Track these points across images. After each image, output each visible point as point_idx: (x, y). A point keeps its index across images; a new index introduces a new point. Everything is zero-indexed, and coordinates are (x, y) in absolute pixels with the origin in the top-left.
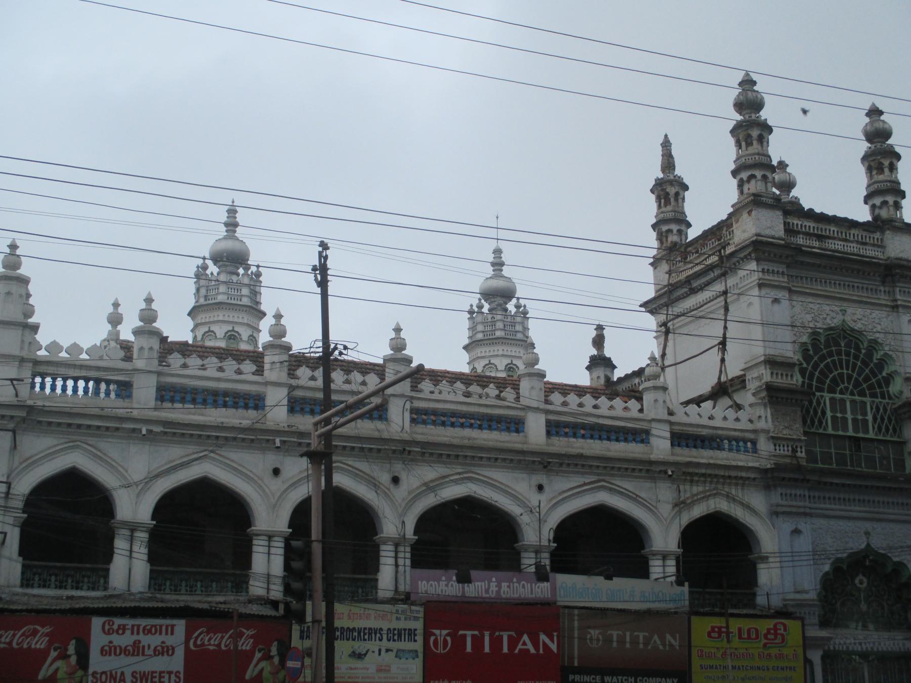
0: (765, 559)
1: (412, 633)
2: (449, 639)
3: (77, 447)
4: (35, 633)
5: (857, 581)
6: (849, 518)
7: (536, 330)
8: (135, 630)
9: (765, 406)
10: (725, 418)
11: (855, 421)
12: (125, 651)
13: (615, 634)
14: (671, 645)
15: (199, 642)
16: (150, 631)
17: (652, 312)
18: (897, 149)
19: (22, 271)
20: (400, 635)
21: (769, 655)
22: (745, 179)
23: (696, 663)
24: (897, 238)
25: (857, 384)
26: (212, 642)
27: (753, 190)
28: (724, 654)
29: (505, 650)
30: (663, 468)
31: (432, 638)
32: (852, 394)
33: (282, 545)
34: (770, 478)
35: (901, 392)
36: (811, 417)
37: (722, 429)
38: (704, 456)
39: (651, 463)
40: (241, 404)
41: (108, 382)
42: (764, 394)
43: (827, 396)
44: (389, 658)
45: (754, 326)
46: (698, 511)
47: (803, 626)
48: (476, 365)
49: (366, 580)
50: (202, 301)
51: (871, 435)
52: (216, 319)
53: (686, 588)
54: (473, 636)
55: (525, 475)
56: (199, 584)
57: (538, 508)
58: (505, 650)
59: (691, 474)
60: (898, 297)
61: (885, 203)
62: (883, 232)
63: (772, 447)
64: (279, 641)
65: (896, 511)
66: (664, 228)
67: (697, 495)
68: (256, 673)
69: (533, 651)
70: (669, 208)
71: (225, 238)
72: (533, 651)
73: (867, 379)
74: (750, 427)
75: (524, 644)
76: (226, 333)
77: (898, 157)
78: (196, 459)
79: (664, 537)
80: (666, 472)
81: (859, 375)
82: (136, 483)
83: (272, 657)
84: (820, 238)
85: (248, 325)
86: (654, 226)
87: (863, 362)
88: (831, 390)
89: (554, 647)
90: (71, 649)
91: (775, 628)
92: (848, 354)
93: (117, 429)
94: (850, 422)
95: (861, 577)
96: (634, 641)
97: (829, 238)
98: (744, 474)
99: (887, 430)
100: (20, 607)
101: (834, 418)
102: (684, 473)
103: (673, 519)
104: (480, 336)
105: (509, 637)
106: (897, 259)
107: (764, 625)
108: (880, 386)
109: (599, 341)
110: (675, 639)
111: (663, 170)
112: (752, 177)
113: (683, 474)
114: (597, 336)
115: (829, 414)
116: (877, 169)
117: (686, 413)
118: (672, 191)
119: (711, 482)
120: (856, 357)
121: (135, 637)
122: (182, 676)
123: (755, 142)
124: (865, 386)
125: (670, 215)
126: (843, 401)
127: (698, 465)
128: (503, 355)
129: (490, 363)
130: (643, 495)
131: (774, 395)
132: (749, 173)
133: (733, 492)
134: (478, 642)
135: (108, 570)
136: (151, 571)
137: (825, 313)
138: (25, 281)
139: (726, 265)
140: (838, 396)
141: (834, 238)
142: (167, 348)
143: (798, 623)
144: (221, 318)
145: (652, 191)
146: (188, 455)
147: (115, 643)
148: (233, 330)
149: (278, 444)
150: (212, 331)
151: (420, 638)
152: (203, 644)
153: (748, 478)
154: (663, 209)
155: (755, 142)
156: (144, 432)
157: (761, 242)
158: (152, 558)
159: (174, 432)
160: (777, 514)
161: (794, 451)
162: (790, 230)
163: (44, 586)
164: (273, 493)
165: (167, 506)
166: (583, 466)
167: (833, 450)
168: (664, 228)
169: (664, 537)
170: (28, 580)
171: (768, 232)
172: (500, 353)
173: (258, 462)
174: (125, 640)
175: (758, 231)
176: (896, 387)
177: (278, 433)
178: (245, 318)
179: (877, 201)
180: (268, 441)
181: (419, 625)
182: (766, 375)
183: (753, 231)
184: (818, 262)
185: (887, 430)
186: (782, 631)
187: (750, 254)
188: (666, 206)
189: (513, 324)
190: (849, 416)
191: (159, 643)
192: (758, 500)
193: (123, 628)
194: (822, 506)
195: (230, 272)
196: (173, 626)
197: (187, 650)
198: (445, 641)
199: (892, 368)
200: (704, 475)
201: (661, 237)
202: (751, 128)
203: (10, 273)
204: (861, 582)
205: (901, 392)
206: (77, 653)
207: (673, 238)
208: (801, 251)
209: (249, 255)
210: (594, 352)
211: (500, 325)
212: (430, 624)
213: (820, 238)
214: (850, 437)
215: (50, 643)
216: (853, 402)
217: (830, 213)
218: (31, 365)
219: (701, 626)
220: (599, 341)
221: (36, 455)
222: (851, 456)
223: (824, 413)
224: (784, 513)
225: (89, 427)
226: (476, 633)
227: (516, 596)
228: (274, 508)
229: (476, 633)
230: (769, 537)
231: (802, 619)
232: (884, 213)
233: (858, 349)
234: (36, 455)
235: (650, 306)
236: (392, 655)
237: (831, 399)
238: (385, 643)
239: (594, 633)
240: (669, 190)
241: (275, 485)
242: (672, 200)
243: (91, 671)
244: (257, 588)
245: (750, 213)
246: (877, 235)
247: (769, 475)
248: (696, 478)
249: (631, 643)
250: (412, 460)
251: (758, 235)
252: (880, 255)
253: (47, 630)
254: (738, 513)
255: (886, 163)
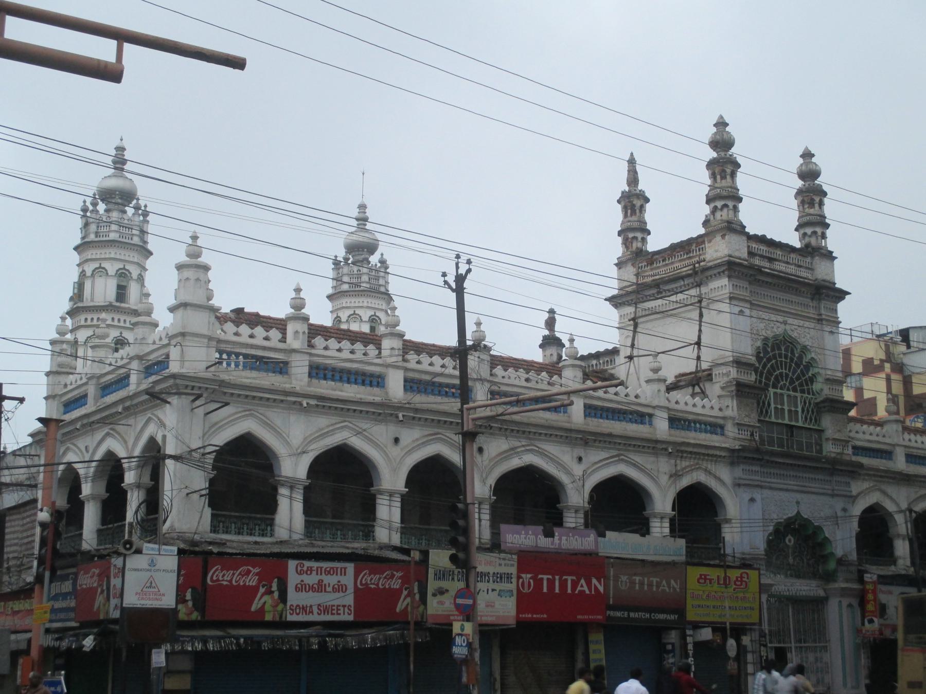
0: (728, 521)
1: (509, 577)
2: (532, 581)
3: (251, 415)
4: (393, 576)
5: (787, 541)
6: (787, 490)
7: (394, 286)
8: (319, 571)
9: (732, 397)
10: (704, 407)
11: (790, 411)
12: (312, 588)
13: (637, 579)
14: (674, 587)
15: (215, 578)
16: (329, 572)
17: (616, 306)
18: (825, 188)
19: (204, 259)
20: (501, 578)
21: (737, 597)
22: (719, 207)
23: (690, 602)
24: (823, 263)
25: (792, 382)
26: (225, 578)
27: (725, 217)
28: (708, 596)
29: (569, 591)
30: (664, 446)
31: (521, 580)
32: (788, 390)
33: (399, 500)
34: (736, 457)
35: (822, 390)
36: (763, 409)
37: (703, 415)
38: (692, 437)
39: (657, 442)
40: (367, 382)
41: (237, 355)
42: (733, 388)
43: (772, 391)
44: (493, 596)
45: (722, 330)
46: (685, 482)
47: (760, 575)
48: (340, 314)
49: (268, 519)
50: (92, 237)
51: (800, 424)
52: (107, 256)
53: (682, 542)
54: (548, 579)
55: (569, 449)
56: (339, 533)
57: (578, 475)
58: (569, 591)
59: (682, 452)
60: (823, 312)
61: (815, 233)
62: (813, 257)
63: (737, 431)
64: (279, 579)
65: (817, 485)
66: (631, 235)
67: (685, 468)
68: (259, 606)
69: (587, 592)
70: (634, 218)
71: (114, 176)
72: (587, 592)
73: (798, 378)
74: (720, 414)
75: (582, 586)
76: (118, 271)
77: (825, 194)
78: (338, 428)
79: (662, 502)
80: (666, 449)
81: (793, 374)
82: (295, 447)
83: (273, 592)
84: (771, 260)
85: (138, 264)
86: (620, 233)
87: (796, 364)
88: (775, 387)
89: (601, 589)
90: (274, 587)
91: (741, 577)
92: (786, 357)
93: (282, 401)
94: (786, 412)
95: (789, 537)
96: (650, 585)
97: (776, 260)
98: (718, 453)
99: (811, 420)
100: (234, 551)
101: (776, 408)
102: (678, 451)
103: (670, 486)
104: (345, 287)
105: (572, 580)
106: (824, 281)
107: (734, 574)
108: (807, 385)
109: (550, 323)
110: (676, 583)
111: (629, 184)
112: (726, 206)
113: (679, 451)
114: (549, 318)
115: (773, 406)
116: (809, 203)
117: (668, 399)
118: (638, 203)
119: (695, 458)
120: (792, 360)
121: (319, 577)
122: (352, 609)
123: (728, 177)
124: (797, 383)
125: (636, 225)
126: (782, 395)
127: (688, 444)
128: (368, 307)
129: (354, 314)
130: (649, 467)
131: (741, 390)
132: (723, 203)
133: (709, 466)
134: (551, 583)
135: (273, 519)
136: (306, 521)
137: (773, 325)
138: (206, 268)
139: (700, 275)
140: (779, 391)
141: (779, 261)
142: (315, 331)
143: (757, 572)
144: (112, 256)
145: (619, 202)
146: (332, 425)
147: (342, 583)
148: (124, 268)
149: (401, 418)
150: (104, 268)
151: (514, 580)
152: (218, 580)
153: (720, 456)
154: (630, 219)
155: (728, 177)
156: (401, 418)
157: (735, 263)
158: (307, 511)
159: (324, 405)
160: (739, 485)
161: (752, 435)
162: (751, 254)
163: (227, 532)
164: (393, 461)
165: (319, 466)
166: (610, 442)
167: (775, 435)
168: (631, 235)
169: (662, 502)
170: (263, 530)
171: (737, 254)
172: (365, 304)
173: (382, 432)
174: (312, 579)
175: (730, 253)
176: (816, 386)
177: (400, 408)
178: (134, 257)
179: (809, 231)
180: (392, 415)
181: (513, 570)
182: (733, 373)
183: (726, 252)
184: (769, 280)
185: (811, 420)
186: (745, 579)
187: (723, 272)
188: (631, 215)
189: (377, 278)
190: (786, 408)
191: (299, 582)
192: (725, 473)
193: (310, 569)
194: (769, 480)
195: (360, 266)
196: (345, 568)
197: (356, 590)
198: (529, 583)
199: (816, 370)
200: (691, 453)
201: (626, 243)
202: (723, 165)
203: (193, 261)
204: (790, 541)
205: (822, 390)
206: (279, 589)
207: (636, 245)
208: (761, 271)
209: (136, 191)
210: (547, 332)
211: (365, 278)
212: (521, 569)
213: (771, 260)
214: (787, 425)
215: (260, 581)
216: (789, 396)
217: (777, 239)
218: (206, 341)
219: (694, 573)
220: (550, 323)
221: (221, 421)
222: (787, 440)
223: (769, 405)
224: (745, 485)
225: (261, 398)
226: (550, 577)
227: (572, 547)
228: (395, 470)
229: (550, 577)
230: (733, 504)
231: (759, 569)
232: (813, 241)
233: (792, 353)
234: (221, 421)
235: (615, 301)
236: (496, 593)
237: (775, 393)
238: (491, 585)
239: (624, 578)
240: (633, 202)
241: (395, 452)
242: (638, 211)
243: (289, 604)
244: (281, 533)
245: (723, 236)
246: (809, 260)
247: (736, 454)
248: (685, 455)
249: (648, 585)
250: (491, 434)
251: (730, 256)
252: (810, 276)
253: (257, 570)
254: (712, 484)
255: (817, 199)
